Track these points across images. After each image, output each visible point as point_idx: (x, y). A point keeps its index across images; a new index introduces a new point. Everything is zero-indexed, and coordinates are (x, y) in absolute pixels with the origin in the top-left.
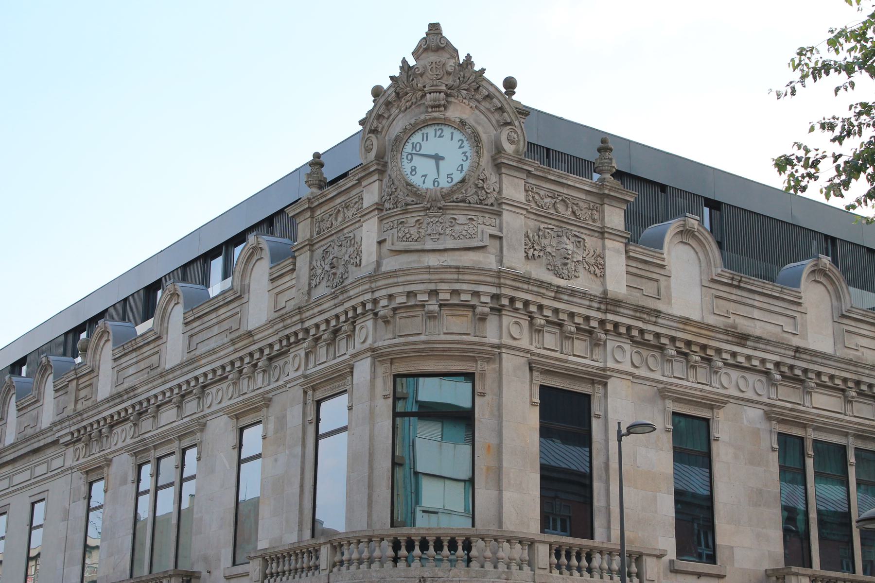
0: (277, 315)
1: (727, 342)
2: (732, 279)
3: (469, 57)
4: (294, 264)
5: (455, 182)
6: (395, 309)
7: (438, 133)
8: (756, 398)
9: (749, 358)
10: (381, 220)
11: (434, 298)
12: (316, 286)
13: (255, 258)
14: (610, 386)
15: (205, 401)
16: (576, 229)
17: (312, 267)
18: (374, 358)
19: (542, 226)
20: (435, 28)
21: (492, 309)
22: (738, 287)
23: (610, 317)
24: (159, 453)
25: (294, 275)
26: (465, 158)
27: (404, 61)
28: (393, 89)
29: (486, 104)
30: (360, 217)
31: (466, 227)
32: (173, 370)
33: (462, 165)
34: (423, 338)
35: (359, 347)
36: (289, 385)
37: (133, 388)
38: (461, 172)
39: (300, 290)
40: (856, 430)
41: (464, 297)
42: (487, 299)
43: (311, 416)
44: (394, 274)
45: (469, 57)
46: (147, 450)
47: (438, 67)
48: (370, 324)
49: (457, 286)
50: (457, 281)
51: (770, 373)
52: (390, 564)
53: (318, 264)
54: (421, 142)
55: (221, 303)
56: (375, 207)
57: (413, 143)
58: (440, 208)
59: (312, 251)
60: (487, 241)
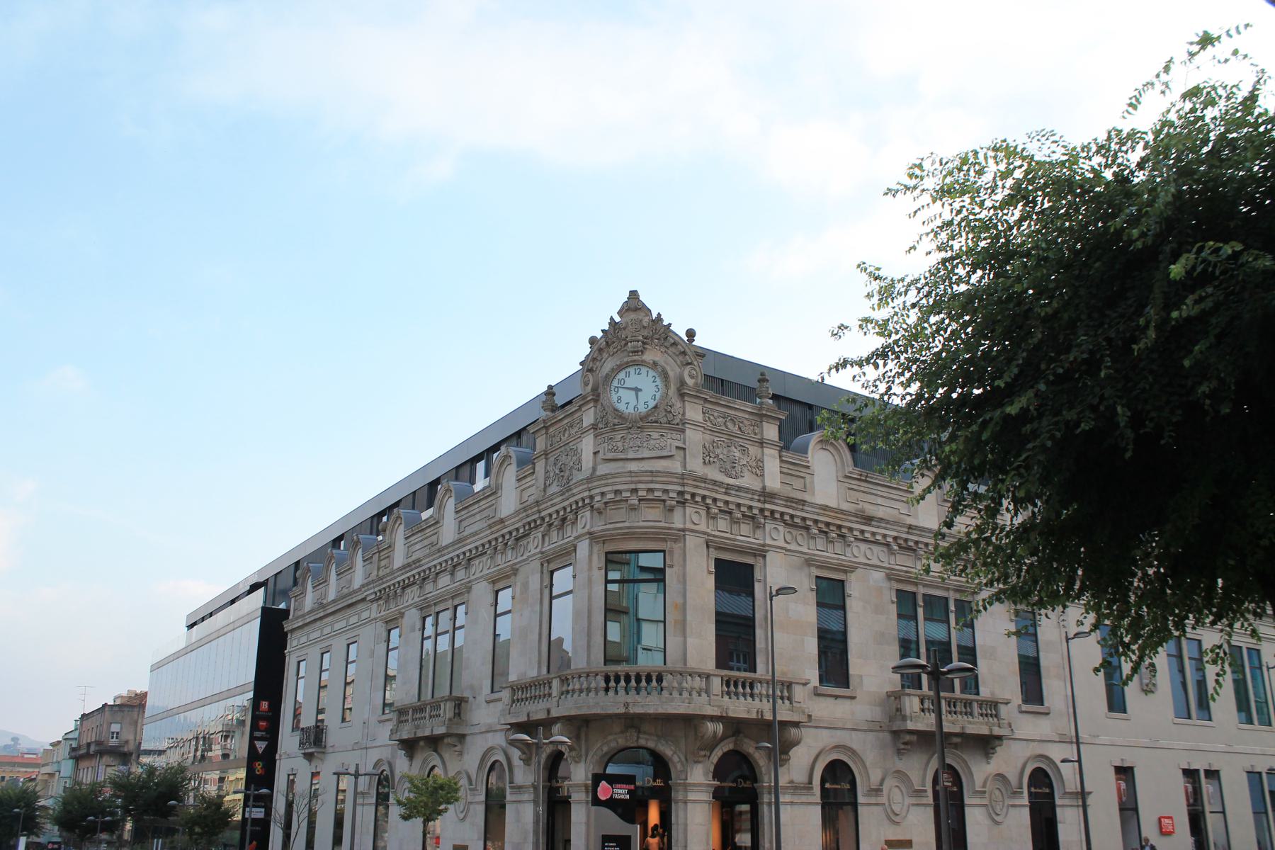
1: (857, 522)
2: (861, 475)
3: (659, 315)
4: (534, 469)
6: (606, 503)
9: (874, 534)
10: (596, 436)
11: (635, 495)
13: (506, 464)
14: (767, 558)
16: (741, 440)
18: (591, 539)
19: (716, 439)
20: (634, 294)
21: (678, 502)
22: (866, 481)
23: (767, 506)
24: (438, 609)
25: (534, 477)
27: (612, 318)
28: (603, 339)
29: (673, 349)
31: (658, 441)
32: (447, 547)
34: (627, 524)
35: (580, 531)
37: (419, 560)
41: (657, 494)
42: (674, 495)
44: (605, 477)
45: (659, 315)
46: (429, 606)
48: (588, 514)
49: (652, 486)
50: (652, 482)
52: (602, 693)
58: (639, 428)
59: (546, 459)
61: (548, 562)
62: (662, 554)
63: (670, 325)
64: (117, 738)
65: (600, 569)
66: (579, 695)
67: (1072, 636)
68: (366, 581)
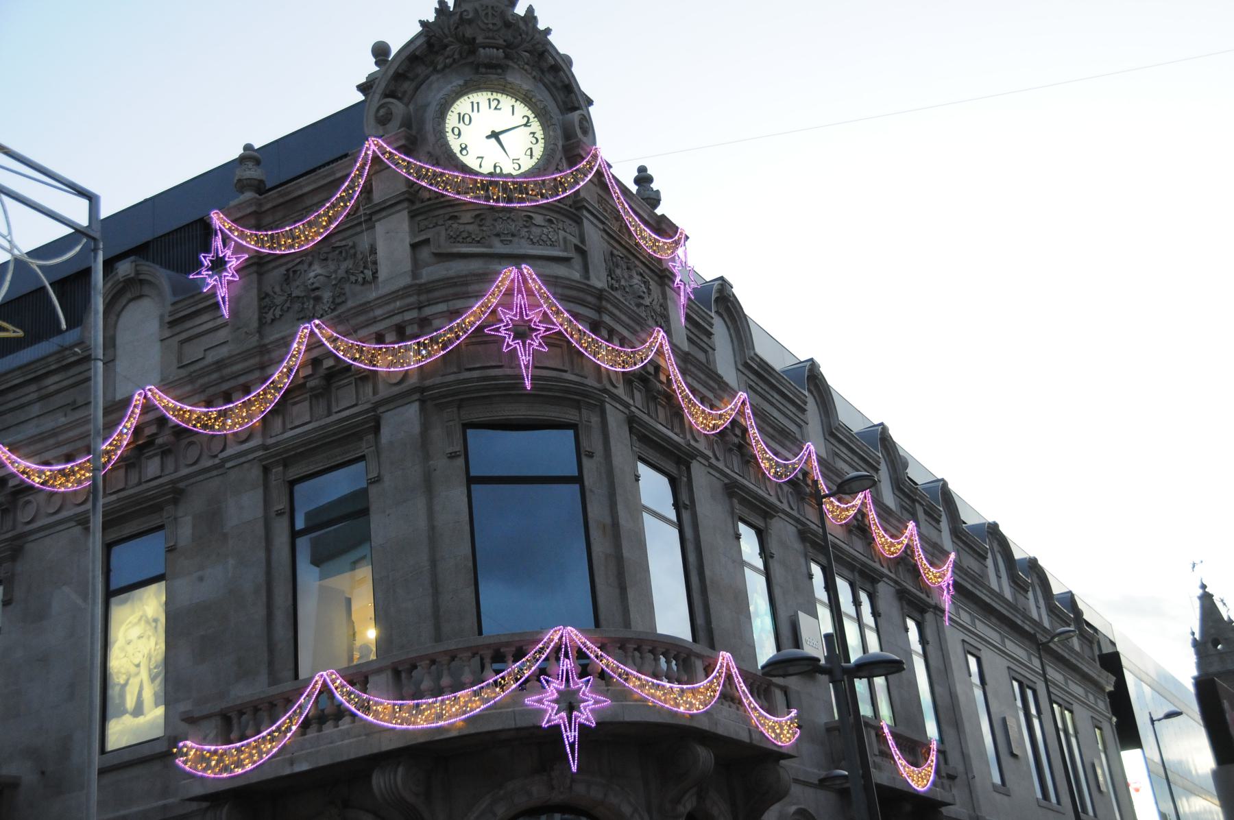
0: (183, 372)
3: (530, 10)
5: (522, 170)
7: (494, 104)
8: (788, 510)
10: (413, 216)
12: (273, 320)
13: (129, 295)
15: (19, 513)
17: (263, 295)
18: (423, 402)
26: (534, 141)
29: (549, 78)
30: (371, 214)
31: (545, 230)
33: (531, 149)
36: (228, 465)
38: (531, 158)
39: (239, 328)
40: (862, 565)
43: (281, 504)
45: (530, 10)
47: (496, 14)
51: (799, 484)
53: (277, 289)
54: (470, 113)
55: (53, 367)
56: (406, 196)
57: (459, 114)
60: (571, 253)
61: (286, 464)
62: (571, 433)
63: (548, 31)
64: (472, 103)
65: (452, 456)
66: (320, 730)
67: (1161, 715)
68: (495, 266)
